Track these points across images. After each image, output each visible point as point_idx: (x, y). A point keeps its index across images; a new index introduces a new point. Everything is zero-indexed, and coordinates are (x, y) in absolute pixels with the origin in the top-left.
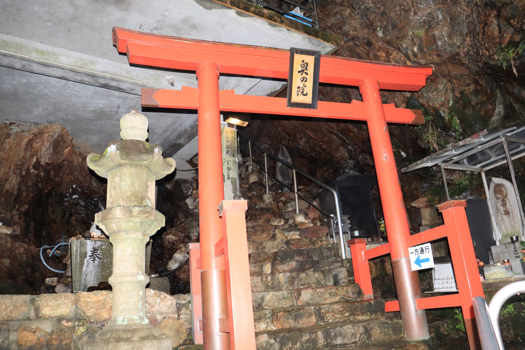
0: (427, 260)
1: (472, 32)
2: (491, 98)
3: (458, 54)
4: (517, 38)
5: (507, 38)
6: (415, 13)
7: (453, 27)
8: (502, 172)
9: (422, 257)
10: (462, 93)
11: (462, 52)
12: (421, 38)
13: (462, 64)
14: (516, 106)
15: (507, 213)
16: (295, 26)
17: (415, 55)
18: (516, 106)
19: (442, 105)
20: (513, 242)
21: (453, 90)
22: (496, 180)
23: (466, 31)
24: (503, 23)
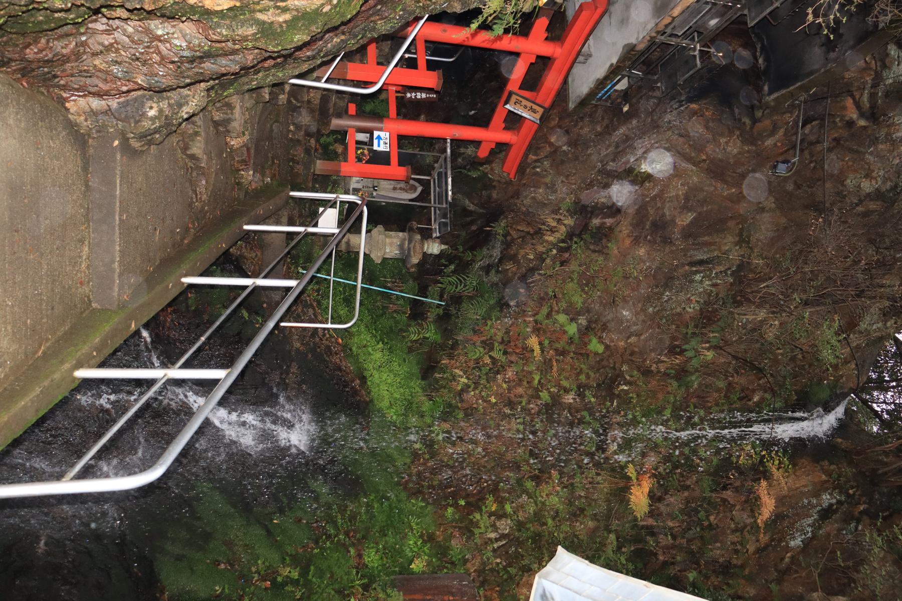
0: (379, 146)
1: (527, 213)
2: (482, 206)
3: (518, 198)
4: (509, 238)
5: (513, 233)
6: (562, 182)
7: (538, 203)
8: (424, 196)
9: (382, 142)
10: (494, 187)
11: (518, 202)
12: (544, 177)
13: (512, 197)
14: (469, 219)
15: (395, 189)
16: (614, 72)
17: (535, 167)
18: (469, 219)
19: (492, 169)
20: (374, 187)
21: (499, 181)
22: (420, 189)
23: (530, 210)
24: (522, 234)
